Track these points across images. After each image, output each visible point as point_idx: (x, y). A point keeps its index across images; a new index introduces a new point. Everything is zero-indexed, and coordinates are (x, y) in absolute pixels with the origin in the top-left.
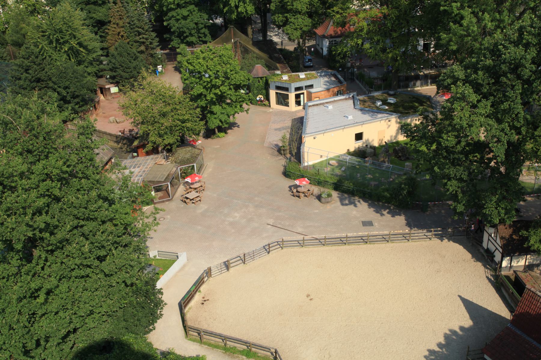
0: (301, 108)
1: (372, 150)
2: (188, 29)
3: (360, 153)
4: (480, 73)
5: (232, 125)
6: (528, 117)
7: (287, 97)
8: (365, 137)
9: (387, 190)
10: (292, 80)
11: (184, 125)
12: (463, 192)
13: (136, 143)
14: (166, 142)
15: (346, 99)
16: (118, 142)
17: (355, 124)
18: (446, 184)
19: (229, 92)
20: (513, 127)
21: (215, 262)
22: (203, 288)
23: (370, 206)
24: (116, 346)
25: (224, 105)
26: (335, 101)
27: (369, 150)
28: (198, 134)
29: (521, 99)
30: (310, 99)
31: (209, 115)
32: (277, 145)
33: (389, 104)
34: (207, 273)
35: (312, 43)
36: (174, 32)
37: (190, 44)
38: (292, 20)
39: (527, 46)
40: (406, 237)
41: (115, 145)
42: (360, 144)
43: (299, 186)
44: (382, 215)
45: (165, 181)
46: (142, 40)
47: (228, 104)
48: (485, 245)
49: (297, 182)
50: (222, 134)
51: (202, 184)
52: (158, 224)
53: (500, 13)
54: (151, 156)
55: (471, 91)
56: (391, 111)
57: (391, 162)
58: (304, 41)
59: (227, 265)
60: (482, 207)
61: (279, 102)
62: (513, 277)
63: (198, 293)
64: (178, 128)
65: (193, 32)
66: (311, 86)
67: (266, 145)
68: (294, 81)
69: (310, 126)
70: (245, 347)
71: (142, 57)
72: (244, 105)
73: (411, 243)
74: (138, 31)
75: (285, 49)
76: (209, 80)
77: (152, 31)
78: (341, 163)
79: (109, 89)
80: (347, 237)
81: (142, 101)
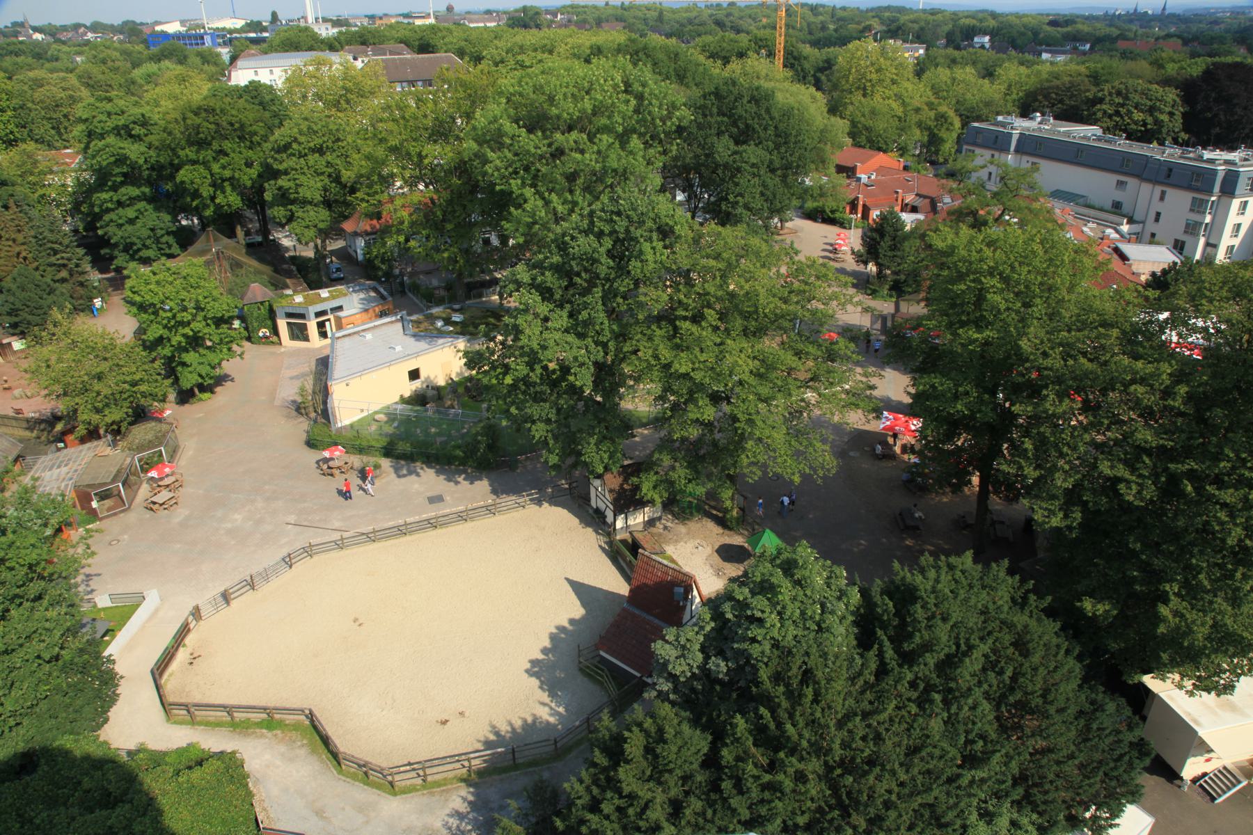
0: (328, 341)
1: (435, 392)
2: (139, 238)
3: (419, 399)
4: (547, 273)
5: (221, 380)
6: (615, 327)
7: (303, 328)
8: (423, 374)
9: (459, 447)
10: (309, 302)
11: (135, 389)
12: (556, 438)
13: (59, 427)
14: (108, 420)
15: (392, 322)
16: (30, 429)
17: (407, 357)
18: (529, 430)
19: (206, 330)
20: (597, 343)
21: (206, 596)
22: (189, 640)
23: (438, 473)
24: (43, 761)
25: (201, 350)
26: (375, 327)
27: (430, 393)
28: (164, 400)
29: (604, 304)
30: (340, 326)
31: (179, 368)
32: (294, 402)
33: (454, 324)
34: (193, 615)
35: (340, 244)
36: (116, 245)
37: (146, 261)
38: (300, 214)
39: (600, 235)
40: (490, 510)
41: (27, 434)
42: (417, 384)
43: (332, 459)
44: (457, 483)
45: (114, 481)
46: (61, 262)
47: (209, 348)
48: (593, 504)
49: (327, 454)
50: (206, 395)
51: (178, 477)
52: (93, 553)
53: (571, 192)
54: (88, 445)
55: (539, 299)
56: (457, 333)
57: (463, 406)
58: (323, 241)
59: (226, 597)
60: (579, 454)
61: (293, 337)
62: (630, 541)
63: (181, 650)
64: (124, 396)
65: (148, 242)
66: (340, 308)
67: (277, 403)
68: (313, 303)
69: (339, 368)
70: (265, 716)
71: (63, 288)
72: (235, 347)
73: (498, 518)
74: (52, 249)
75: (300, 257)
76: (169, 315)
77: (78, 246)
78: (391, 416)
79: (10, 344)
80: (406, 524)
81: (60, 360)
